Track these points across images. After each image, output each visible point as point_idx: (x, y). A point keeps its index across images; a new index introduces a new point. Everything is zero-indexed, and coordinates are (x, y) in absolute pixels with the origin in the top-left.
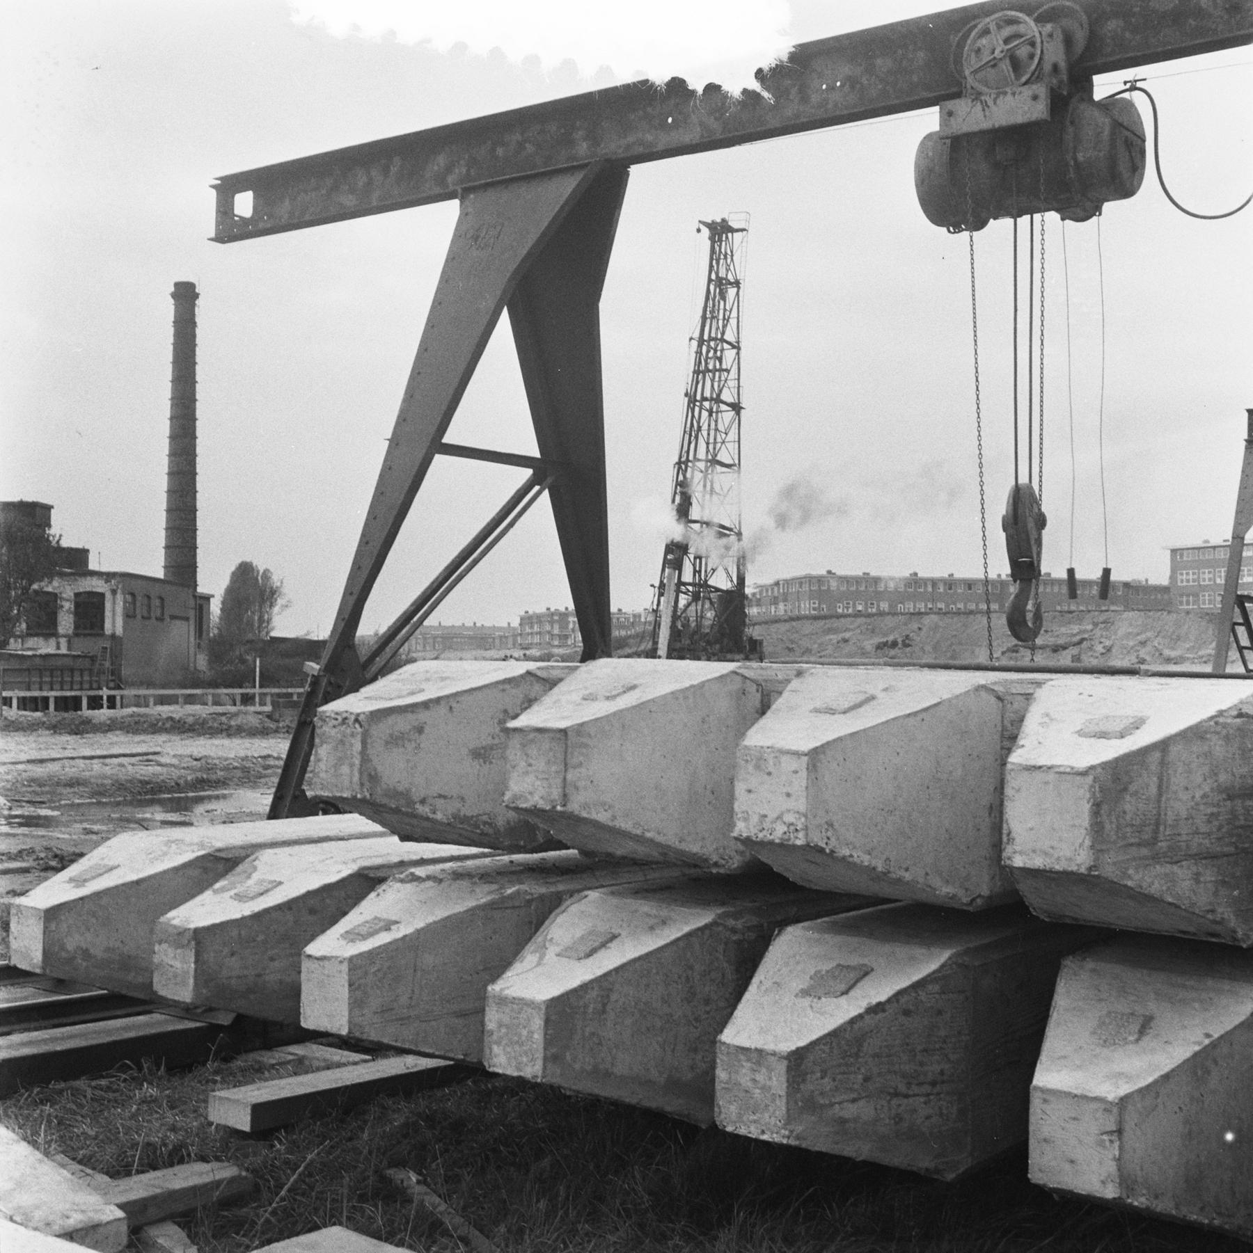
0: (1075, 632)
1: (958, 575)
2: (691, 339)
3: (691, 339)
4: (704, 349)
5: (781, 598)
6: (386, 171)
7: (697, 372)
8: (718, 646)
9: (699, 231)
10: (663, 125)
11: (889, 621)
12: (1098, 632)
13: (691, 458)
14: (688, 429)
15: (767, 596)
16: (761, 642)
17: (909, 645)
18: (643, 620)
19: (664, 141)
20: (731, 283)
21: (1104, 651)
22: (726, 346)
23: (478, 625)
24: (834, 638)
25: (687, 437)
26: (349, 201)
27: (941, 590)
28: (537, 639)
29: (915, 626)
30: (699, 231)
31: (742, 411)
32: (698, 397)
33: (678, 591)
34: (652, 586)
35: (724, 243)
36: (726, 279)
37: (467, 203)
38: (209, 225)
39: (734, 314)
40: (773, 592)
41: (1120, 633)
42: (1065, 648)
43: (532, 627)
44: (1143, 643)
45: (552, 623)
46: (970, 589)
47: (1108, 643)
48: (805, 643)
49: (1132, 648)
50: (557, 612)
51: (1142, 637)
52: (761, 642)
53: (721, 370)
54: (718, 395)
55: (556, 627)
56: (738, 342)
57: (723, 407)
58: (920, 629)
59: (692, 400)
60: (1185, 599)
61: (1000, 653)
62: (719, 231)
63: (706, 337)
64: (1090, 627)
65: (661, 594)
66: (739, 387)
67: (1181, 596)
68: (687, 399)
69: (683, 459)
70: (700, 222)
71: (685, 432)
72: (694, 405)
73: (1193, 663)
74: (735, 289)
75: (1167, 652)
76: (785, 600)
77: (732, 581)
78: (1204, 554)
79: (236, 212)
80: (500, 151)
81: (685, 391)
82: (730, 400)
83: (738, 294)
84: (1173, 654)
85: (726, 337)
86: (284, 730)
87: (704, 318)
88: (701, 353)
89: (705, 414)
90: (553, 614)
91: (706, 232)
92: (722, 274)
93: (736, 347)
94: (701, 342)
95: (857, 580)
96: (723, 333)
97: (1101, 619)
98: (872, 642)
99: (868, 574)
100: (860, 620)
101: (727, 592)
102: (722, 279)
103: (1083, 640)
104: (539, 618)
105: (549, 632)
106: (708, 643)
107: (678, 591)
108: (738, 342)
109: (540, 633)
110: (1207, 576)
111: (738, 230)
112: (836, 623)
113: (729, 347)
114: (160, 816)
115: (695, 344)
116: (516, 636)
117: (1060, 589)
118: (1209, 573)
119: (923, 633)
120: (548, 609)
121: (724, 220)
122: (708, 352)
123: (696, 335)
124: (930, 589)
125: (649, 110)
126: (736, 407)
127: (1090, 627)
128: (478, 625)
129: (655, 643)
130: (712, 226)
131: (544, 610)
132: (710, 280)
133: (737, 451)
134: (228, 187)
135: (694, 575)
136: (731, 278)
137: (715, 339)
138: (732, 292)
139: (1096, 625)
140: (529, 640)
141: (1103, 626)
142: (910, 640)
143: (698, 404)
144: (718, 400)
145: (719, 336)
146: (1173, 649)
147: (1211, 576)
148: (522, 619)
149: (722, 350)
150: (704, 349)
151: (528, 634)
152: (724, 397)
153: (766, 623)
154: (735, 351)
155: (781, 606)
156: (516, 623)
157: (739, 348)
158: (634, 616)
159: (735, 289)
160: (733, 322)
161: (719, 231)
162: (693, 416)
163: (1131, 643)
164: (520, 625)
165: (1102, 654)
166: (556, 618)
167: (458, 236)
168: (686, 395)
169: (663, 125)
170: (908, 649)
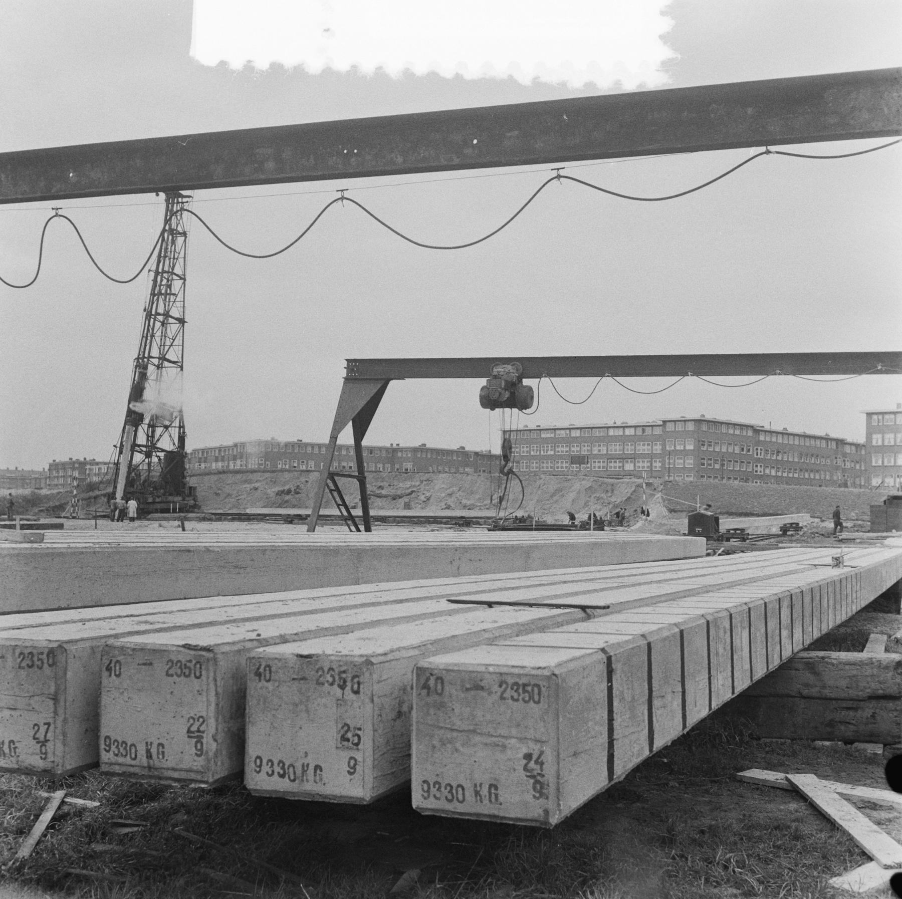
0: (408, 486)
4: (159, 278)
5: (238, 456)
7: (153, 294)
8: (162, 491)
11: (287, 475)
13: (146, 355)
14: (145, 335)
15: (195, 457)
16: (195, 488)
17: (298, 493)
20: (180, 233)
24: (248, 486)
25: (144, 340)
28: (61, 481)
29: (303, 479)
31: (186, 324)
32: (153, 312)
33: (133, 450)
34: (115, 446)
36: (176, 230)
40: (233, 452)
41: (436, 488)
42: (400, 497)
44: (450, 495)
46: (371, 453)
47: (428, 494)
48: (227, 490)
50: (78, 461)
51: (449, 491)
52: (195, 488)
53: (171, 294)
54: (168, 312)
56: (184, 275)
58: (307, 482)
59: (149, 315)
63: (160, 270)
64: (418, 483)
65: (121, 452)
66: (184, 307)
68: (145, 313)
71: (143, 337)
72: (150, 318)
73: (480, 509)
74: (183, 238)
75: (464, 501)
76: (241, 458)
77: (174, 444)
78: (588, 432)
81: (143, 308)
82: (177, 316)
83: (185, 241)
84: (468, 503)
85: (175, 271)
88: (157, 281)
89: (158, 324)
90: (74, 463)
92: (174, 226)
93: (183, 278)
95: (293, 445)
96: (173, 269)
97: (425, 478)
98: (273, 490)
99: (301, 441)
100: (267, 475)
101: (171, 452)
102: (174, 230)
103: (413, 492)
104: (63, 466)
105: (70, 476)
106: (155, 488)
107: (133, 450)
108: (184, 275)
109: (64, 476)
110: (525, 449)
112: (250, 476)
114: (356, 659)
116: (46, 478)
117: (427, 455)
118: (527, 447)
119: (309, 485)
120: (71, 459)
122: (162, 281)
126: (182, 321)
129: (115, 487)
131: (67, 460)
133: (180, 352)
135: (148, 440)
136: (180, 229)
137: (168, 272)
138: (180, 240)
139: (422, 482)
140: (55, 482)
142: (300, 489)
146: (469, 499)
147: (528, 449)
151: (55, 477)
153: (199, 475)
155: (238, 462)
157: (185, 280)
159: (183, 238)
162: (149, 325)
163: (443, 495)
165: (424, 502)
166: (77, 465)
168: (145, 310)
170: (297, 496)
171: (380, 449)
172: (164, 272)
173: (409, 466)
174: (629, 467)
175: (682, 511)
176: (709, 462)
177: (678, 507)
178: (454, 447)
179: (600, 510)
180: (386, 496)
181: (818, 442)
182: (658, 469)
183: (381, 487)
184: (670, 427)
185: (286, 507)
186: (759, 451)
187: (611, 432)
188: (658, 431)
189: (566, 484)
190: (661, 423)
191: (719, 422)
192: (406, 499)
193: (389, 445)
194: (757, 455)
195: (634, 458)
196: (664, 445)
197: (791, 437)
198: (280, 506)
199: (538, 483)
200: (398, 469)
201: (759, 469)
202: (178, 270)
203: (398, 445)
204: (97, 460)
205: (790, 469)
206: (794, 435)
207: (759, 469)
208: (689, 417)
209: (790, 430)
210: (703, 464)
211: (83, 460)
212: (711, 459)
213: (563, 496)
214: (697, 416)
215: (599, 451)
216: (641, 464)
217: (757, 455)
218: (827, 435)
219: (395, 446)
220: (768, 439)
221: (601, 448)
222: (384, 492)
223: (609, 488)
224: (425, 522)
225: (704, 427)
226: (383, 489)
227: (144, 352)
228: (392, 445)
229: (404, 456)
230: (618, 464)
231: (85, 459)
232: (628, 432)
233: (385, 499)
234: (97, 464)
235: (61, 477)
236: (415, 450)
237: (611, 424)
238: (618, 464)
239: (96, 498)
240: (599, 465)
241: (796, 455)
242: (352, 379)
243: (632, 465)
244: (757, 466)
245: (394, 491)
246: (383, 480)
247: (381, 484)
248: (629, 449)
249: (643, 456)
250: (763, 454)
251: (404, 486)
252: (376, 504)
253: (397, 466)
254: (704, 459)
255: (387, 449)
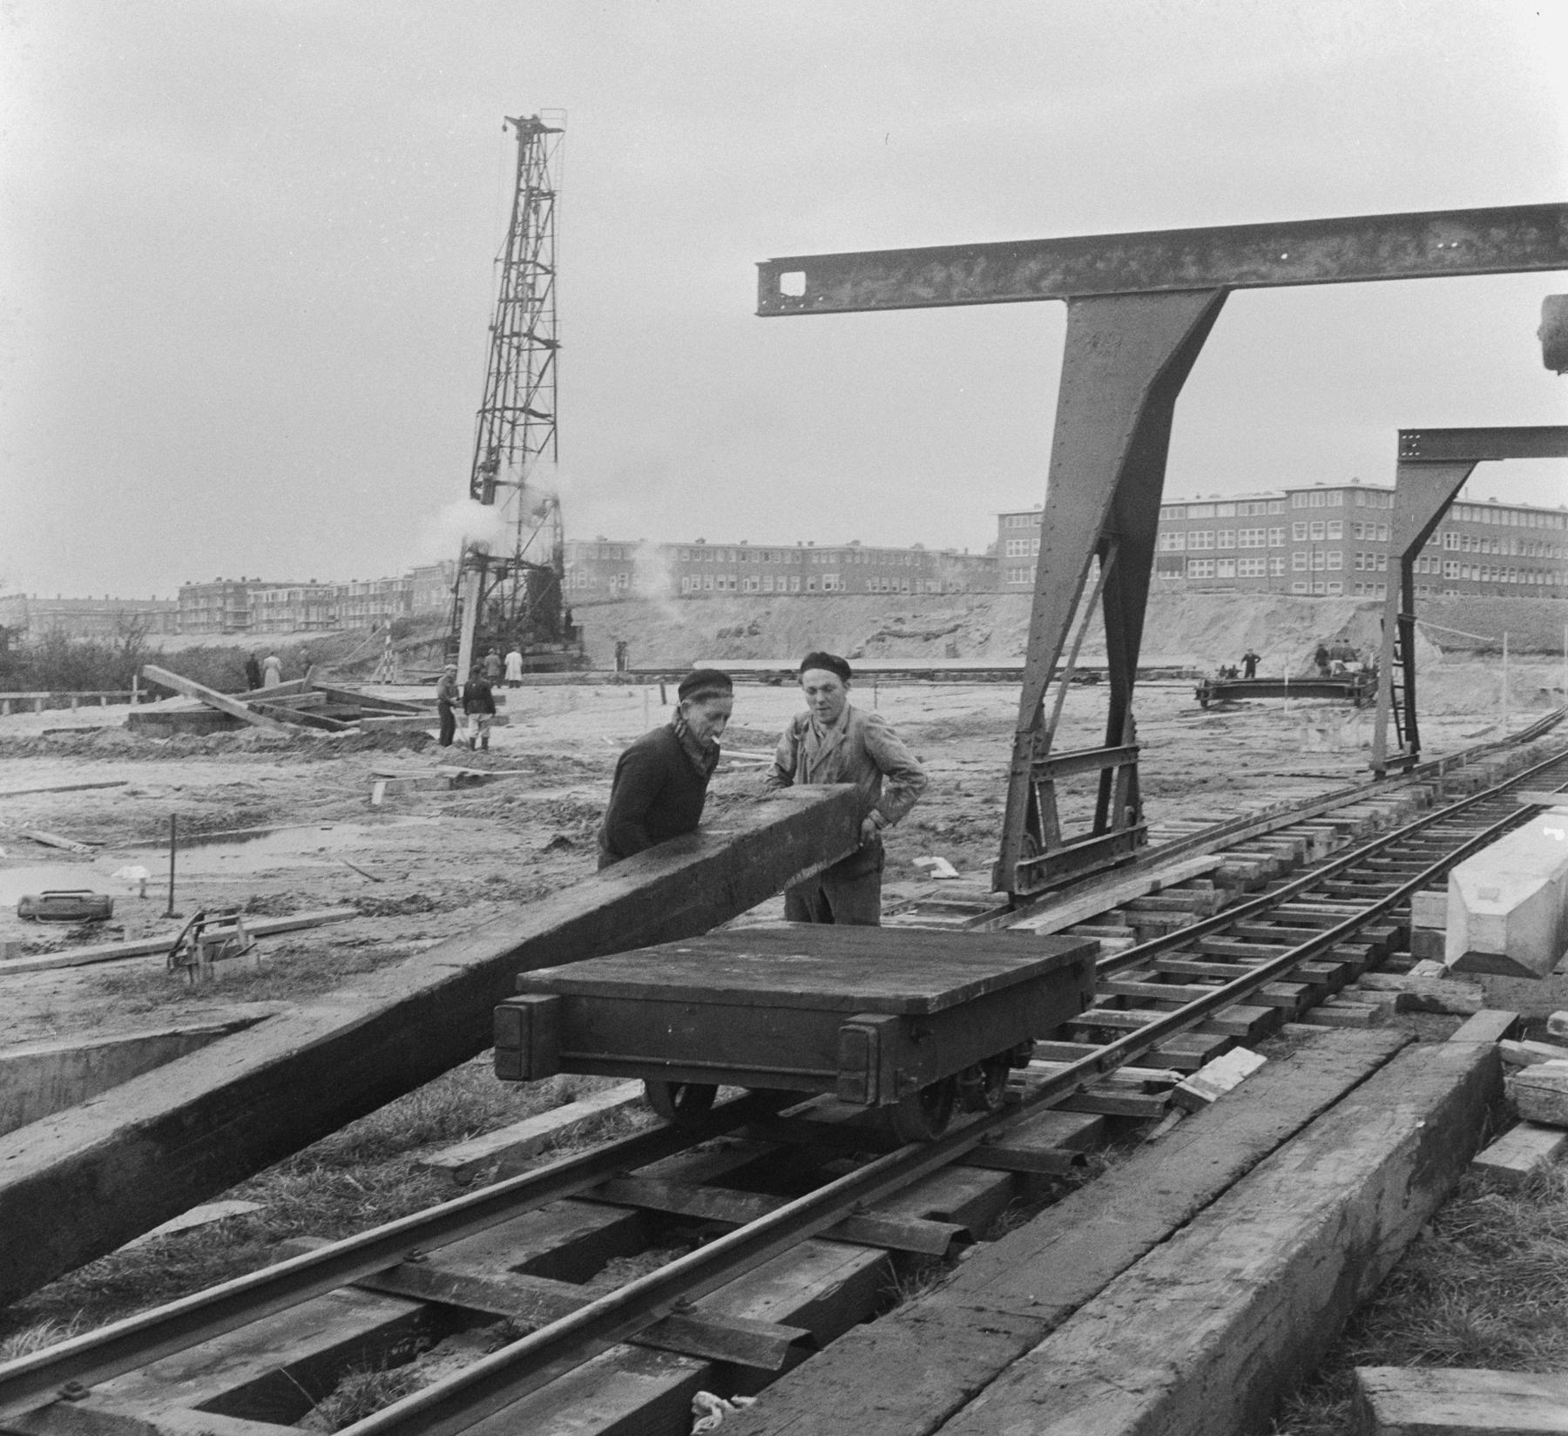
0: (948, 617)
1: (751, 543)
2: (496, 260)
3: (496, 260)
6: (969, 271)
8: (531, 635)
9: (505, 129)
10: (1278, 260)
12: (973, 618)
13: (499, 405)
18: (351, 594)
19: (1278, 273)
20: (544, 194)
21: (982, 639)
22: (539, 270)
23: (112, 598)
25: (493, 380)
26: (926, 293)
27: (734, 560)
30: (505, 129)
32: (507, 332)
35: (535, 146)
36: (538, 189)
37: (1074, 310)
38: (753, 303)
39: (548, 232)
42: (938, 636)
43: (197, 603)
45: (225, 597)
46: (767, 558)
47: (986, 630)
49: (1013, 636)
50: (229, 584)
53: (533, 300)
55: (230, 601)
56: (552, 265)
57: (537, 345)
60: (1014, 572)
61: (864, 641)
62: (530, 130)
63: (515, 258)
64: (964, 612)
66: (554, 321)
67: (1010, 569)
68: (491, 334)
69: (488, 407)
70: (507, 118)
74: (549, 202)
79: (783, 290)
80: (1100, 265)
82: (544, 337)
83: (551, 208)
86: (204, 751)
87: (512, 235)
88: (508, 278)
90: (225, 586)
91: (513, 130)
93: (550, 271)
94: (509, 264)
97: (976, 604)
109: (208, 610)
111: (552, 131)
113: (543, 271)
115: (501, 266)
119: (774, 617)
121: (535, 118)
123: (502, 255)
124: (720, 559)
125: (1263, 245)
126: (552, 345)
127: (964, 612)
128: (112, 598)
129: (456, 631)
130: (520, 123)
132: (519, 190)
134: (771, 271)
136: (544, 188)
138: (545, 205)
139: (971, 609)
140: (192, 619)
141: (979, 610)
143: (506, 340)
144: (530, 335)
145: (529, 257)
148: (182, 591)
149: (535, 275)
150: (514, 274)
151: (191, 611)
152: (539, 332)
154: (549, 277)
156: (175, 596)
157: (554, 275)
158: (340, 589)
159: (549, 202)
160: (547, 241)
161: (530, 130)
163: (1011, 631)
164: (180, 599)
167: (1072, 340)
169: (1278, 260)
171: (782, 551)
172: (523, 261)
173: (833, 578)
174: (1226, 571)
175: (1463, 650)
176: (1370, 560)
177: (1456, 644)
178: (907, 546)
179: (1294, 651)
180: (912, 635)
181: (1549, 520)
182: (1278, 574)
183: (899, 620)
184: (1298, 503)
185: (737, 658)
186: (1452, 539)
187: (1193, 513)
188: (1277, 510)
189: (1228, 608)
190: (1283, 495)
191: (1383, 491)
192: (946, 640)
193: (794, 544)
194: (1449, 545)
195: (1233, 556)
196: (1288, 532)
197: (1505, 514)
198: (725, 657)
199: (1179, 609)
200: (812, 586)
201: (1452, 570)
202: (543, 259)
203: (811, 543)
204: (264, 581)
205: (1504, 569)
206: (1510, 509)
207: (1452, 570)
208: (1330, 483)
209: (1503, 500)
210: (1358, 565)
211: (240, 581)
212: (1371, 556)
213: (1226, 628)
214: (1347, 483)
215: (1173, 545)
216: (1247, 568)
217: (1449, 545)
218: (1562, 507)
219: (805, 545)
220: (1466, 518)
221: (1175, 541)
222: (906, 628)
223: (1306, 613)
224: (1002, 678)
225: (1360, 500)
226: (903, 623)
227: (495, 395)
228: (800, 543)
229: (824, 562)
230: (1205, 568)
231: (244, 579)
232: (1224, 512)
233: (911, 640)
234: (265, 587)
235: (203, 610)
236: (842, 554)
237: (1191, 499)
238: (1205, 568)
239: (417, 648)
240: (1252, 568)
241: (1513, 543)
242: (1411, 462)
243: (1232, 569)
244: (1448, 565)
245: (923, 626)
246: (902, 607)
247: (901, 615)
248: (1226, 542)
249: (1251, 553)
250: (1458, 543)
251: (939, 617)
252: (895, 649)
253: (810, 581)
254: (1360, 555)
255: (793, 551)
